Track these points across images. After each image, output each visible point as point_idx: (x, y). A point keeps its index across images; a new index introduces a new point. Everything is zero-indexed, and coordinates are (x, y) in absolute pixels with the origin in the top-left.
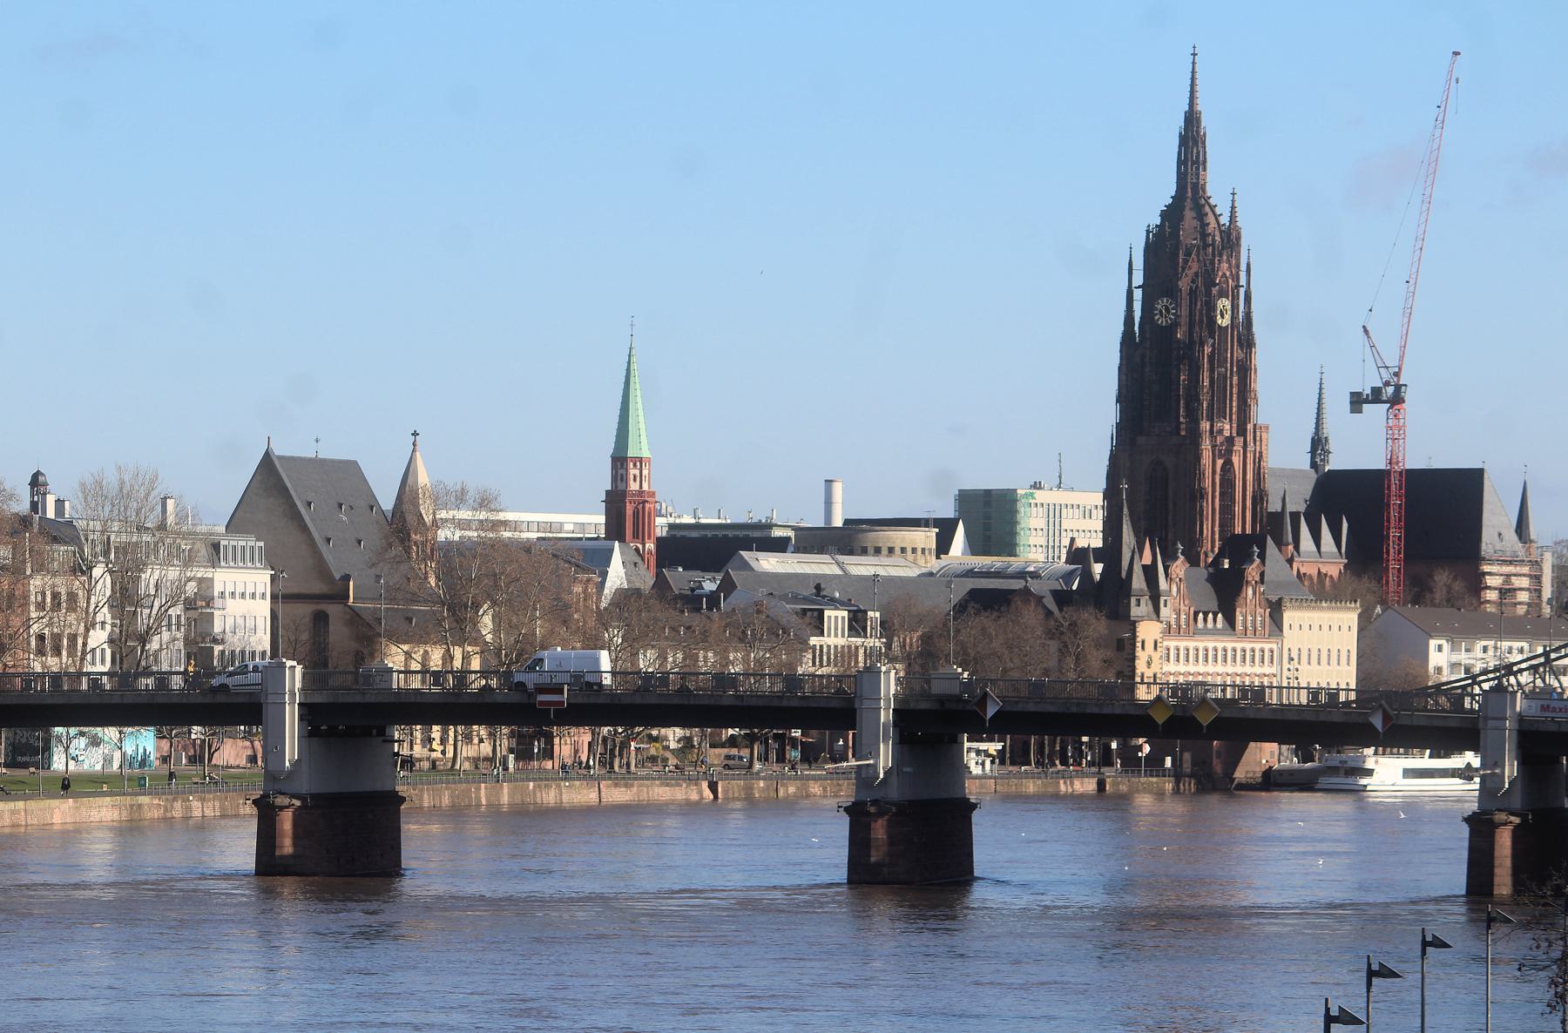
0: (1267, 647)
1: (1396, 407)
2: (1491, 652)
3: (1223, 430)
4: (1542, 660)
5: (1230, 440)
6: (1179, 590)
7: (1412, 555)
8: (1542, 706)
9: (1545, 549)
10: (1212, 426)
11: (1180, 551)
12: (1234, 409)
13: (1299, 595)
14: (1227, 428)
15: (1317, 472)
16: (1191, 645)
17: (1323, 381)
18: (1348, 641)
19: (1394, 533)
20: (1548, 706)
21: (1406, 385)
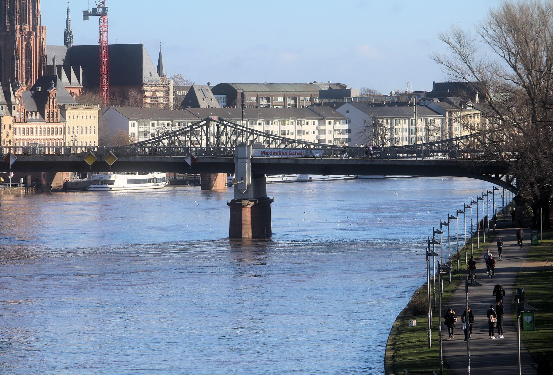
0: (59, 126)
1: (104, 17)
2: (156, 126)
3: (26, 29)
4: (189, 129)
5: (29, 33)
6: (20, 102)
7: (112, 83)
8: (262, 152)
9: (170, 79)
10: (21, 27)
11: (54, 84)
12: (30, 19)
13: (71, 103)
14: (27, 27)
15: (67, 47)
16: (26, 126)
17: (69, 6)
18: (95, 123)
19: (104, 73)
20: (264, 152)
21: (108, 8)
